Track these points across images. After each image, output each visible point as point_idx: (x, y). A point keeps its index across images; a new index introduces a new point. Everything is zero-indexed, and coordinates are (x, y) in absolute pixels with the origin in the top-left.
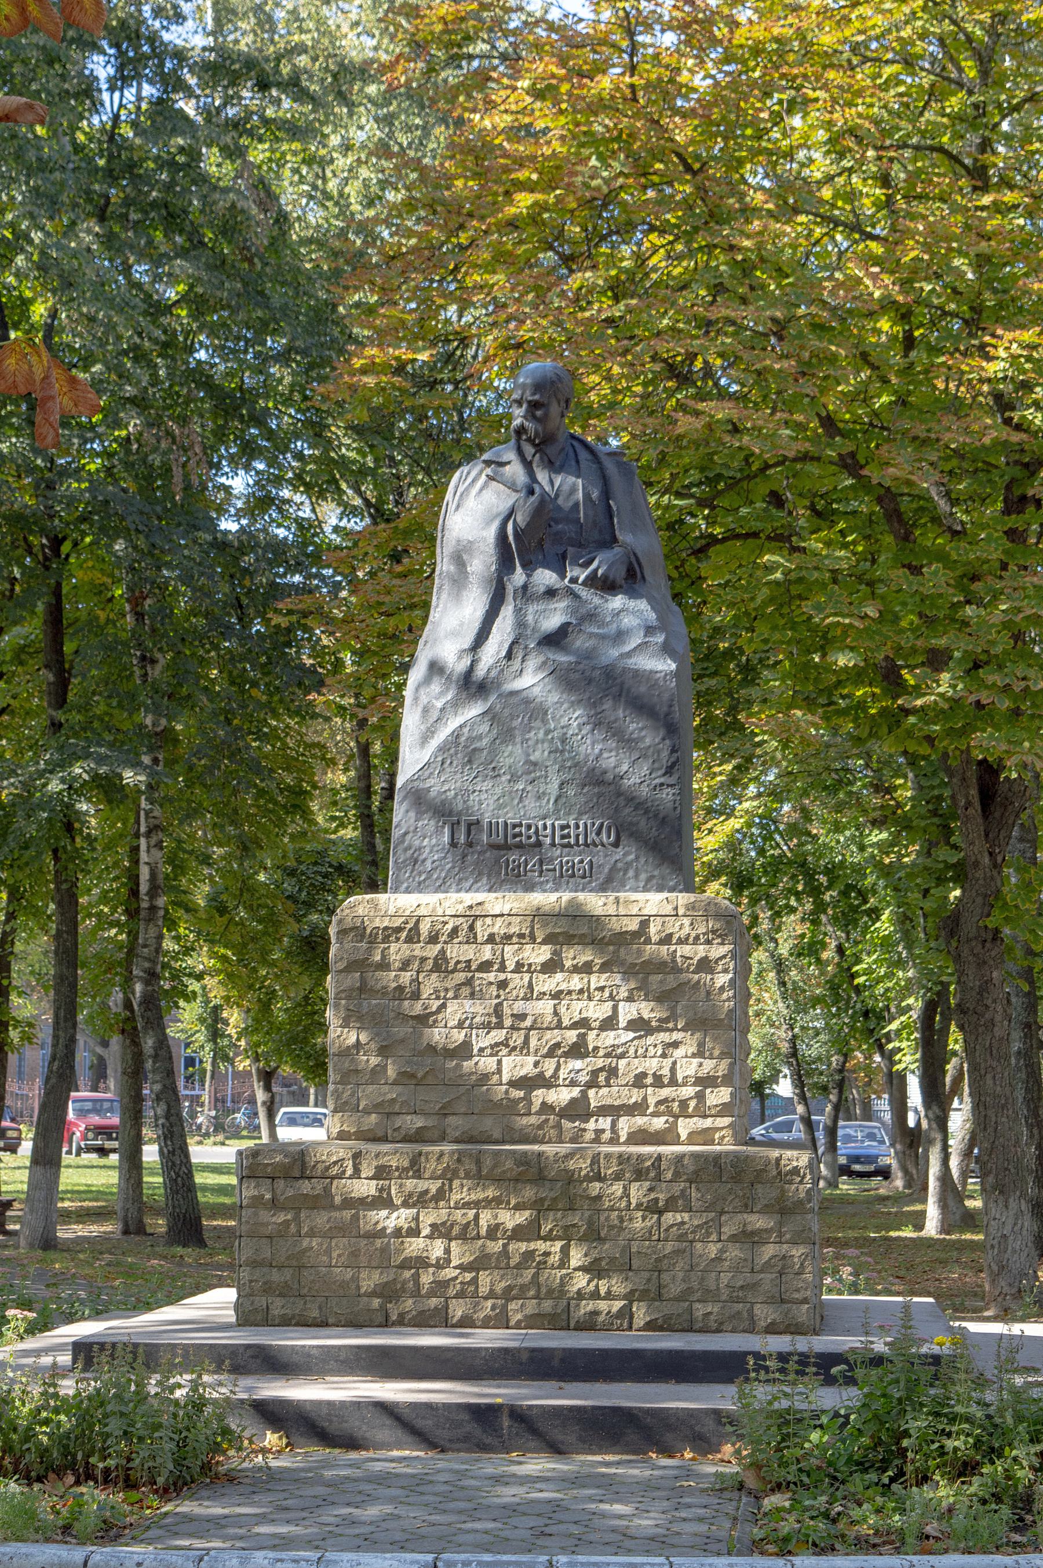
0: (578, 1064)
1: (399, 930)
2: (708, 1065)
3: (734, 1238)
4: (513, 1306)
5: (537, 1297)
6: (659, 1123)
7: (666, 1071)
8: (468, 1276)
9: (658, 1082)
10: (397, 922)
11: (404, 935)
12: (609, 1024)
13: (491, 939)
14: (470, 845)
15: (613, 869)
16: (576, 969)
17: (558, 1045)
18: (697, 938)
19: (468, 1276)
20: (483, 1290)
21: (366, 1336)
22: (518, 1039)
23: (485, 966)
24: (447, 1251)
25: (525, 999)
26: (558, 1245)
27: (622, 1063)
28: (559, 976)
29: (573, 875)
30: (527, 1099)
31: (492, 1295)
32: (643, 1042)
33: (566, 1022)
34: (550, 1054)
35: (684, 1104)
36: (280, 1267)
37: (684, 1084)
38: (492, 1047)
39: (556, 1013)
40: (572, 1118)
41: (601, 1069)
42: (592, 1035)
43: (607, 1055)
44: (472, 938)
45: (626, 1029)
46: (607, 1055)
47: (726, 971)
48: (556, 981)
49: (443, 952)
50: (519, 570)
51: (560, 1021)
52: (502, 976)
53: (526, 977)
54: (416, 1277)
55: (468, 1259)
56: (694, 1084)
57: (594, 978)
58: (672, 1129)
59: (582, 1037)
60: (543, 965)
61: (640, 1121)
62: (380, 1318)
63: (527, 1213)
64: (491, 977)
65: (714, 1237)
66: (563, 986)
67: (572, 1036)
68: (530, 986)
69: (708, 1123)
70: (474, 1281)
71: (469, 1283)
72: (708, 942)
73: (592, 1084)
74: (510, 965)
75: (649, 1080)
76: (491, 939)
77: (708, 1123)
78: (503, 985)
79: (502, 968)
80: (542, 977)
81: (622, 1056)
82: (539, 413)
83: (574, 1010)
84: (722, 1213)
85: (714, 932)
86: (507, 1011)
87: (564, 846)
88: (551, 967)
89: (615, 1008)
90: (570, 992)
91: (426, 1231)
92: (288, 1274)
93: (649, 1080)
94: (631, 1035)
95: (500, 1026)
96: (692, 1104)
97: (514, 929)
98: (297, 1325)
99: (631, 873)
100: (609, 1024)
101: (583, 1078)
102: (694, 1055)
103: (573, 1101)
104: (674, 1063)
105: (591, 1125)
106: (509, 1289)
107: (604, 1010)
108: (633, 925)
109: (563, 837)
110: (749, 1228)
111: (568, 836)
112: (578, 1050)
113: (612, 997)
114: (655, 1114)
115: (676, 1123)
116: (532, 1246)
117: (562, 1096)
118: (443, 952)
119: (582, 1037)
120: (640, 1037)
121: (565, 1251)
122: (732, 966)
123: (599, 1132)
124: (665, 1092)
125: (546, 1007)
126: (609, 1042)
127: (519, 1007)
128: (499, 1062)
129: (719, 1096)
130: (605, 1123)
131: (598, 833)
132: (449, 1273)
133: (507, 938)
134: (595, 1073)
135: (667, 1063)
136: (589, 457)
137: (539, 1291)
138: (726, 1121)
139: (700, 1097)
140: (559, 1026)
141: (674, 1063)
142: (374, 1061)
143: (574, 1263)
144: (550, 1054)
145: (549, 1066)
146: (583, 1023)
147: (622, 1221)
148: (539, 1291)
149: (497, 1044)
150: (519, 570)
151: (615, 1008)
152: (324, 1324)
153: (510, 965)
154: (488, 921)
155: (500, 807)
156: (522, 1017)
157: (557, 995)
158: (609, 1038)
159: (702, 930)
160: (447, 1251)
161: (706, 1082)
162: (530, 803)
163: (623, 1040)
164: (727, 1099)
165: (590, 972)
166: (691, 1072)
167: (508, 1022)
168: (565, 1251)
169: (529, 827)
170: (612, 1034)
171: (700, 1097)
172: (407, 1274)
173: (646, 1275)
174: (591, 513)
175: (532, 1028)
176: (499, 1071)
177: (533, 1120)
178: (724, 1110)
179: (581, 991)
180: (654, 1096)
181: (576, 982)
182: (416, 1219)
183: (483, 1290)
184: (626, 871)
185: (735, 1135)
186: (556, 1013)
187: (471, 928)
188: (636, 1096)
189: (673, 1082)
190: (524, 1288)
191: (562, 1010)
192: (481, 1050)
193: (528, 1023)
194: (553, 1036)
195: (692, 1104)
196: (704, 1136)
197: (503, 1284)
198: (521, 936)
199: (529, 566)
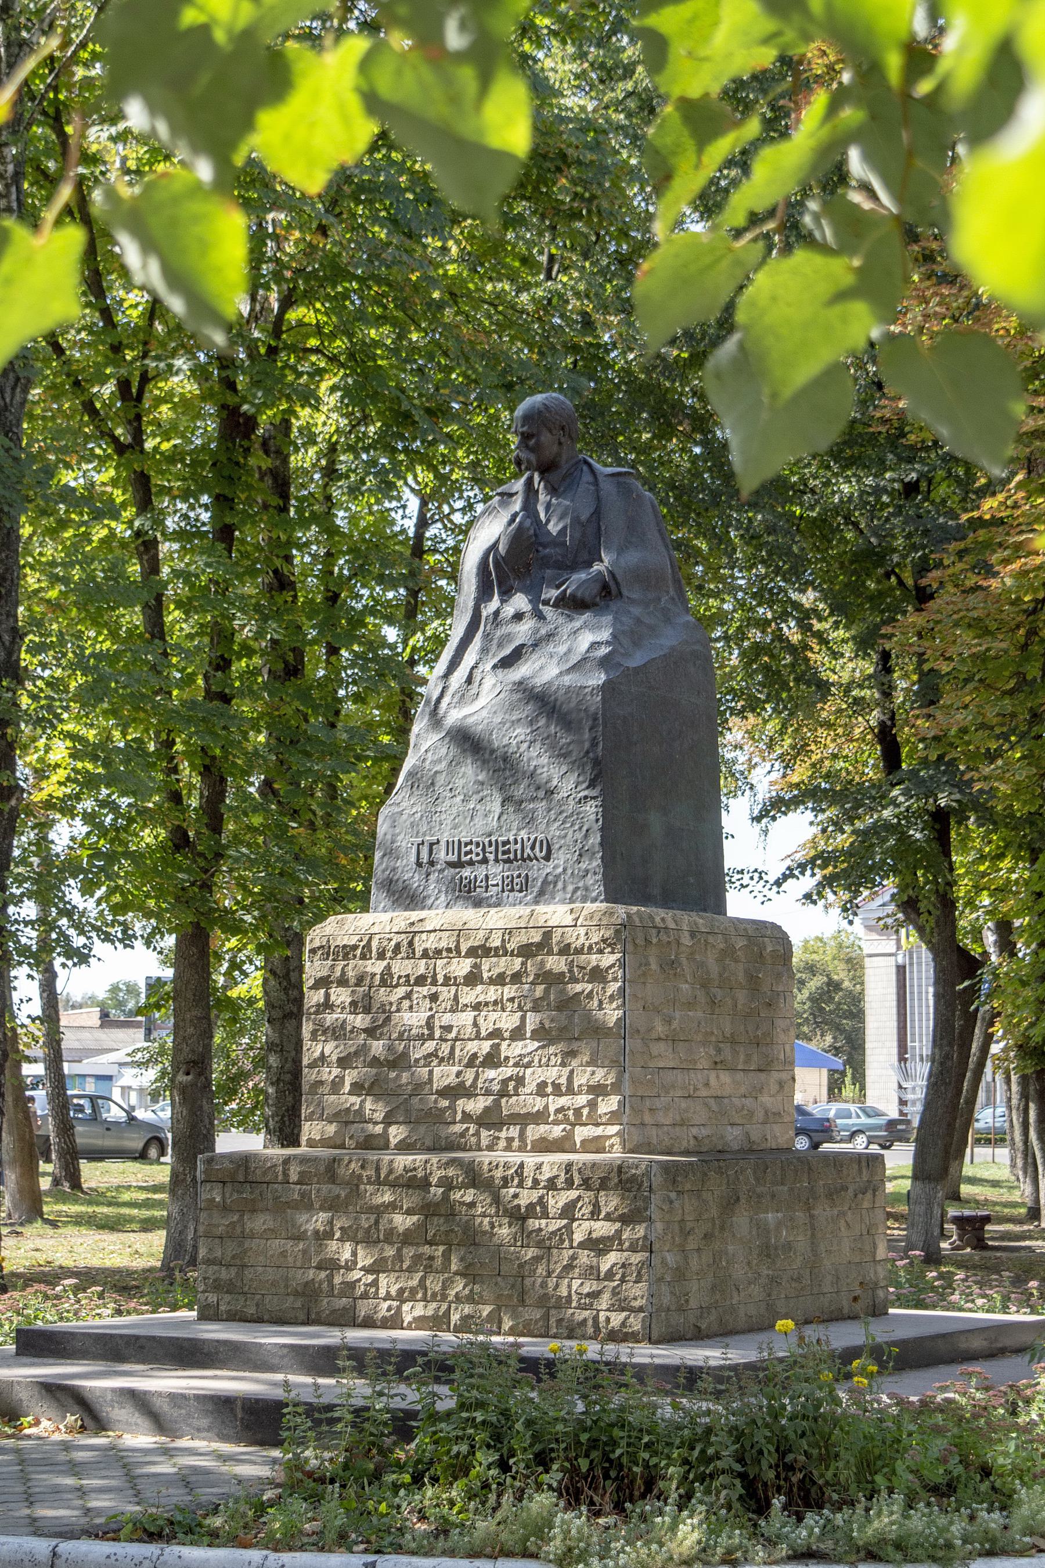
0: (491, 1073)
1: (355, 947)
2: (600, 1073)
3: (582, 1245)
4: (406, 1307)
5: (424, 1299)
6: (557, 1131)
7: (563, 1081)
8: (370, 1278)
9: (557, 1091)
10: (353, 941)
11: (359, 952)
12: (517, 1034)
13: (425, 954)
14: (432, 863)
15: (545, 882)
16: (492, 981)
17: (475, 1056)
18: (590, 948)
19: (370, 1278)
20: (382, 1292)
21: (372, 1340)
22: (445, 1048)
23: (421, 981)
24: (354, 1254)
25: (453, 1011)
26: (441, 1248)
27: (529, 1071)
28: (479, 988)
29: (512, 890)
30: (452, 1107)
31: (388, 1297)
32: (546, 1051)
33: (483, 1034)
34: (470, 1064)
35: (578, 1112)
36: (228, 1266)
37: (580, 1093)
38: (425, 1057)
39: (475, 1024)
40: (489, 1126)
41: (510, 1079)
42: (504, 1045)
43: (516, 1065)
44: (411, 955)
45: (532, 1039)
46: (516, 1065)
47: (615, 979)
48: (469, 995)
49: (388, 967)
50: (496, 597)
51: (478, 1032)
52: (434, 989)
53: (453, 989)
54: (330, 1278)
55: (369, 1261)
56: (588, 1093)
57: (506, 989)
58: (569, 1136)
59: (496, 1048)
60: (465, 977)
61: (543, 1128)
62: (302, 1317)
63: (415, 1218)
64: (424, 990)
65: (566, 1244)
66: (481, 999)
67: (486, 1046)
68: (456, 998)
69: (599, 1131)
70: (375, 1283)
71: (370, 1285)
72: (601, 952)
73: (503, 1093)
74: (440, 979)
75: (549, 1089)
76: (425, 954)
77: (599, 1131)
78: (434, 998)
79: (434, 983)
80: (466, 989)
81: (528, 1065)
82: (532, 442)
83: (490, 1020)
84: (574, 1220)
85: (604, 941)
86: (437, 1024)
87: (505, 861)
88: (473, 979)
89: (523, 1019)
90: (487, 1004)
91: (337, 1235)
92: (233, 1271)
93: (549, 1089)
94: (536, 1044)
95: (431, 1037)
96: (585, 1112)
97: (443, 944)
98: (241, 1320)
99: (560, 885)
100: (517, 1034)
101: (496, 1087)
102: (588, 1064)
103: (487, 1109)
104: (572, 1072)
105: (503, 1134)
106: (401, 1291)
107: (514, 1021)
108: (537, 938)
109: (504, 853)
110: (594, 1235)
111: (508, 852)
112: (492, 1060)
113: (520, 1008)
114: (556, 1123)
115: (572, 1131)
116: (421, 1250)
117: (476, 1105)
118: (388, 967)
119: (496, 1048)
120: (543, 1047)
121: (447, 1257)
122: (620, 974)
123: (510, 1140)
124: (563, 1101)
125: (466, 1018)
126: (517, 1052)
127: (447, 1019)
128: (431, 1072)
129: (609, 1104)
130: (514, 1132)
131: (533, 848)
132: (356, 1275)
133: (438, 952)
134: (505, 1082)
135: (566, 1071)
136: (591, 479)
137: (425, 1294)
138: (613, 1129)
139: (592, 1105)
140: (478, 1037)
141: (572, 1072)
142: (336, 1071)
143: (454, 1267)
144: (470, 1064)
145: (469, 1075)
146: (496, 1034)
147: (493, 1227)
148: (425, 1294)
149: (430, 1055)
150: (496, 597)
151: (523, 1019)
152: (259, 1320)
153: (440, 979)
154: (424, 936)
155: (455, 827)
156: (448, 1028)
157: (477, 1007)
158: (517, 1049)
159: (595, 938)
160: (354, 1254)
161: (598, 1090)
162: (479, 821)
163: (529, 1049)
164: (615, 1107)
165: (504, 985)
166: (584, 1081)
167: (437, 1035)
168: (447, 1257)
169: (478, 845)
170: (521, 1043)
171: (592, 1105)
172: (323, 1275)
173: (511, 1280)
174: (578, 535)
175: (456, 1039)
176: (430, 1080)
177: (458, 1128)
178: (614, 1117)
179: (495, 1003)
180: (555, 1103)
181: (492, 993)
182: (331, 1223)
183: (382, 1292)
184: (555, 883)
185: (623, 1143)
186: (475, 1024)
187: (411, 944)
188: (539, 1103)
189: (570, 1091)
190: (413, 1291)
191: (481, 1020)
192: (417, 1060)
193: (453, 1035)
194: (472, 1047)
195: (585, 1112)
196: (595, 1145)
197: (397, 1286)
198: (449, 950)
199: (506, 594)
